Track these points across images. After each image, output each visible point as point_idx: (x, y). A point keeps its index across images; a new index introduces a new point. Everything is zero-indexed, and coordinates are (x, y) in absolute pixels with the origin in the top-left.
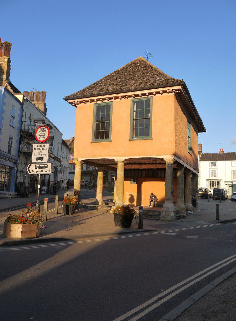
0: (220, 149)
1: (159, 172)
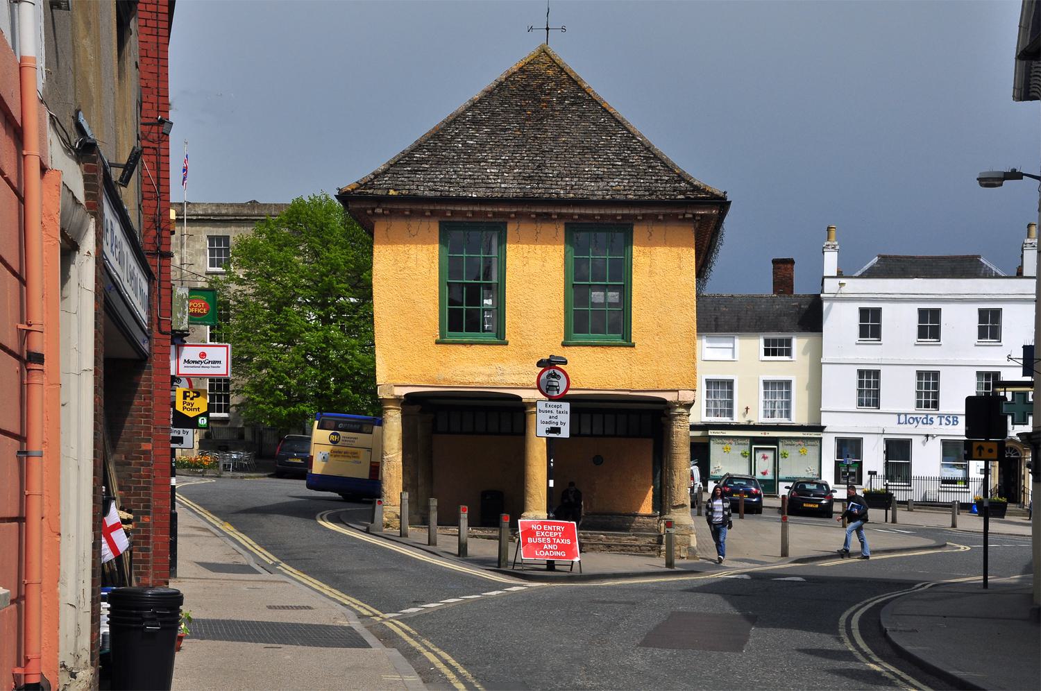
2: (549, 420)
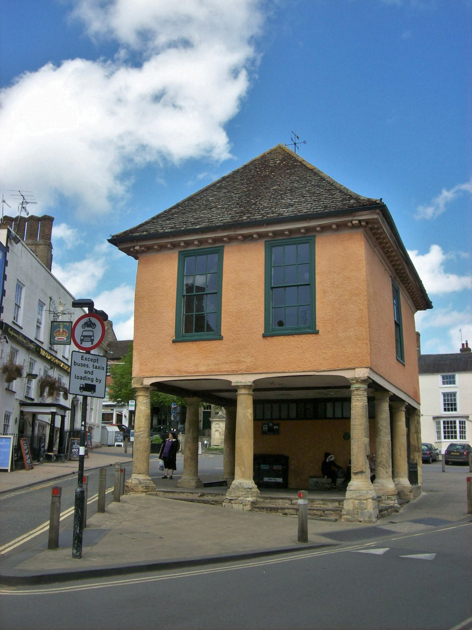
0: (463, 345)
1: (329, 406)
2: (84, 375)
